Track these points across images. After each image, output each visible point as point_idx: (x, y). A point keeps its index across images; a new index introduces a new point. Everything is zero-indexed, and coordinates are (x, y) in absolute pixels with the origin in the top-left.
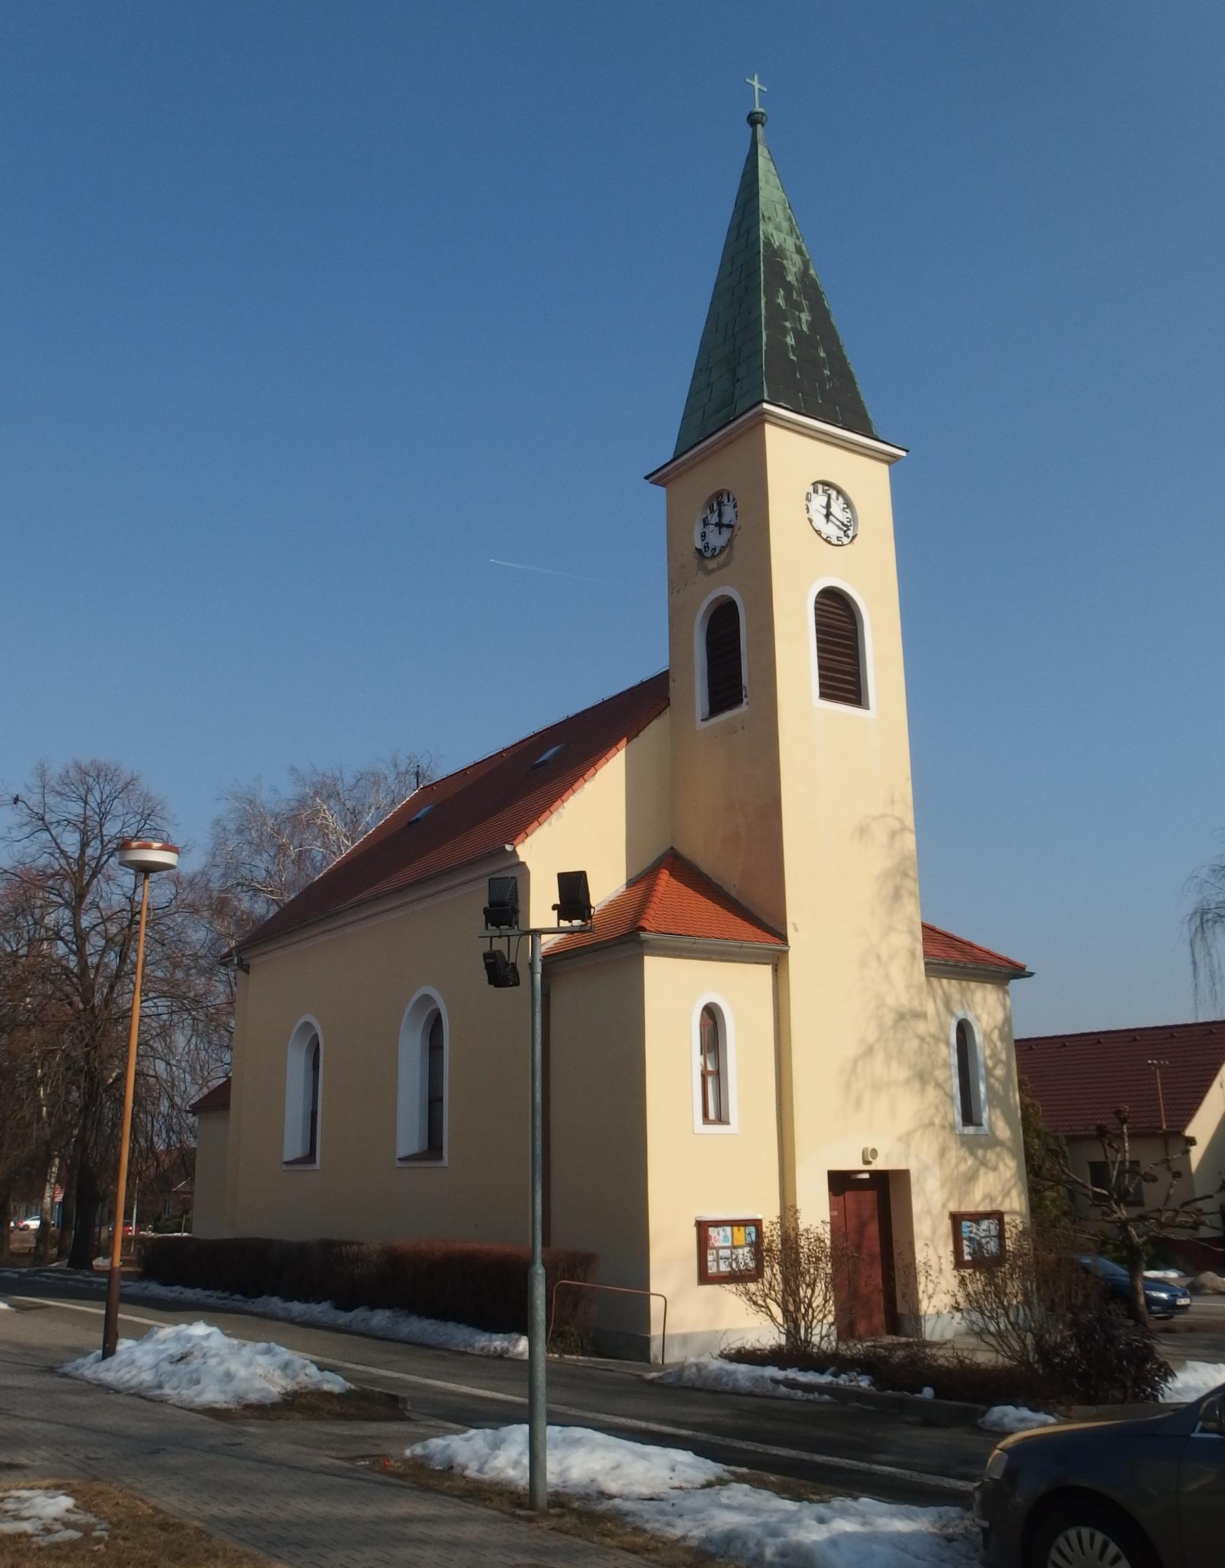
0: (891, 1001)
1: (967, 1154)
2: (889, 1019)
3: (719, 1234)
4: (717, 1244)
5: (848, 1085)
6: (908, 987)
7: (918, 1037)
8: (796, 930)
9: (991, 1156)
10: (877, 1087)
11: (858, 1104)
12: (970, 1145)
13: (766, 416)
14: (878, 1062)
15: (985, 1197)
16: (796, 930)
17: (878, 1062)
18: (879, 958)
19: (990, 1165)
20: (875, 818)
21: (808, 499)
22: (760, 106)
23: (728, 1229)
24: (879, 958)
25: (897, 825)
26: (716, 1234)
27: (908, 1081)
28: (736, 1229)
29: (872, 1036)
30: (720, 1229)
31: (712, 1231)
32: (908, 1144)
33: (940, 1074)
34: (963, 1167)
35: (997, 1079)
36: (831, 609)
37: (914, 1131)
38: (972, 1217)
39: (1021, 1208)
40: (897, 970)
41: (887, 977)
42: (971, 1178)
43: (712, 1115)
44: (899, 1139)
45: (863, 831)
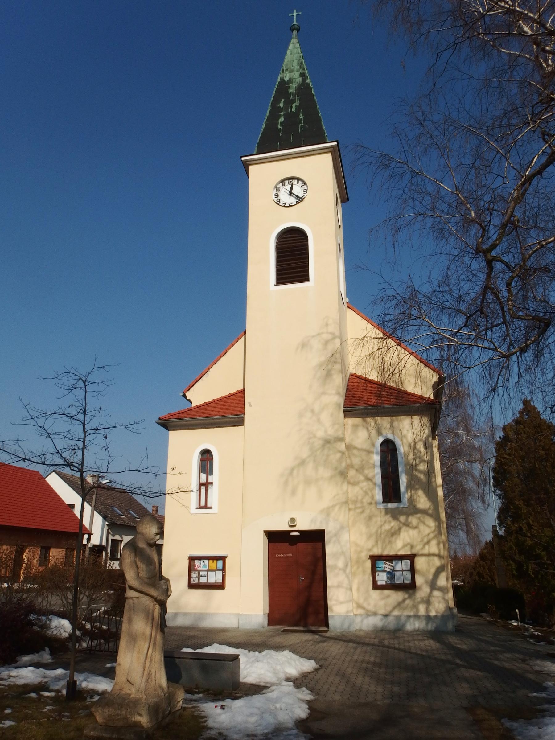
0: (320, 434)
1: (391, 519)
2: (318, 443)
3: (200, 564)
4: (198, 569)
5: (286, 483)
6: (334, 424)
7: (340, 452)
8: (250, 405)
9: (413, 520)
10: (308, 482)
11: (294, 492)
12: (395, 514)
13: (247, 163)
14: (310, 469)
15: (405, 546)
16: (250, 405)
17: (310, 469)
18: (313, 411)
19: (411, 525)
20: (313, 337)
21: (278, 189)
22: (297, 22)
23: (206, 561)
24: (313, 411)
25: (330, 337)
26: (199, 564)
27: (332, 477)
28: (211, 561)
29: (305, 453)
30: (202, 561)
31: (197, 562)
32: (328, 515)
33: (369, 472)
34: (387, 527)
35: (421, 472)
36: (289, 239)
37: (334, 506)
38: (388, 558)
39: (440, 550)
40: (325, 417)
41: (319, 421)
42: (395, 533)
43: (203, 504)
44: (322, 511)
45: (304, 345)
